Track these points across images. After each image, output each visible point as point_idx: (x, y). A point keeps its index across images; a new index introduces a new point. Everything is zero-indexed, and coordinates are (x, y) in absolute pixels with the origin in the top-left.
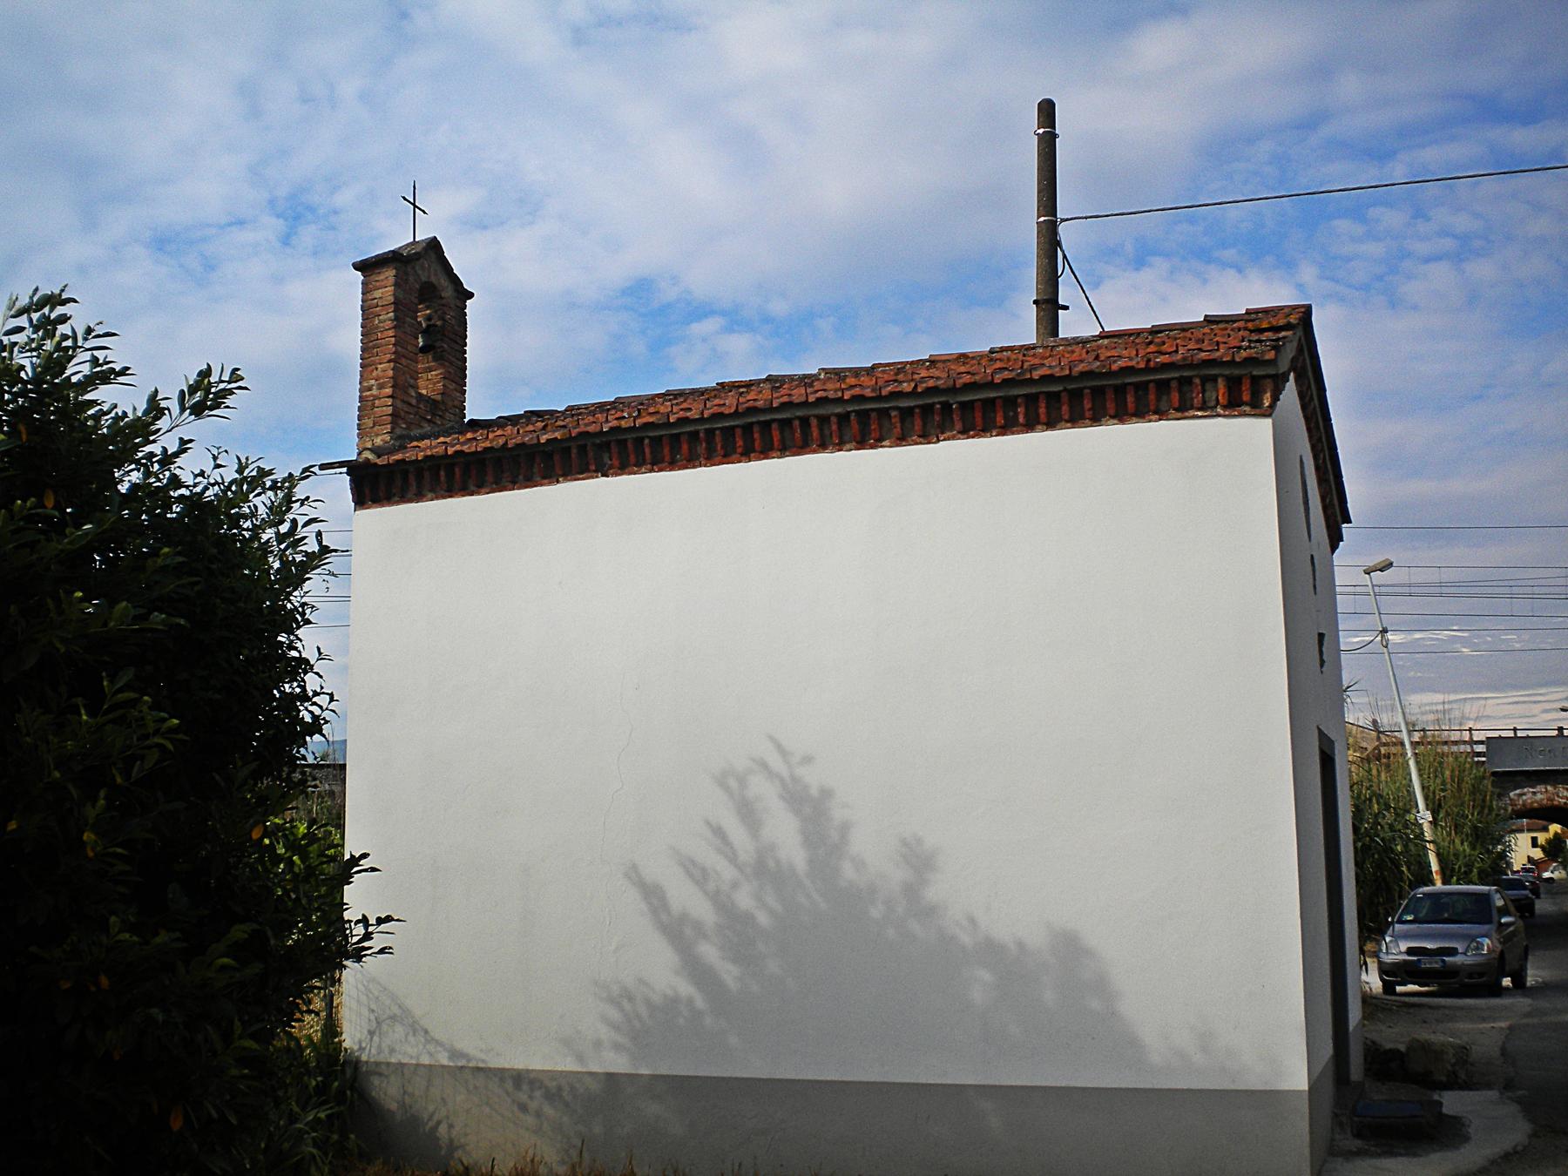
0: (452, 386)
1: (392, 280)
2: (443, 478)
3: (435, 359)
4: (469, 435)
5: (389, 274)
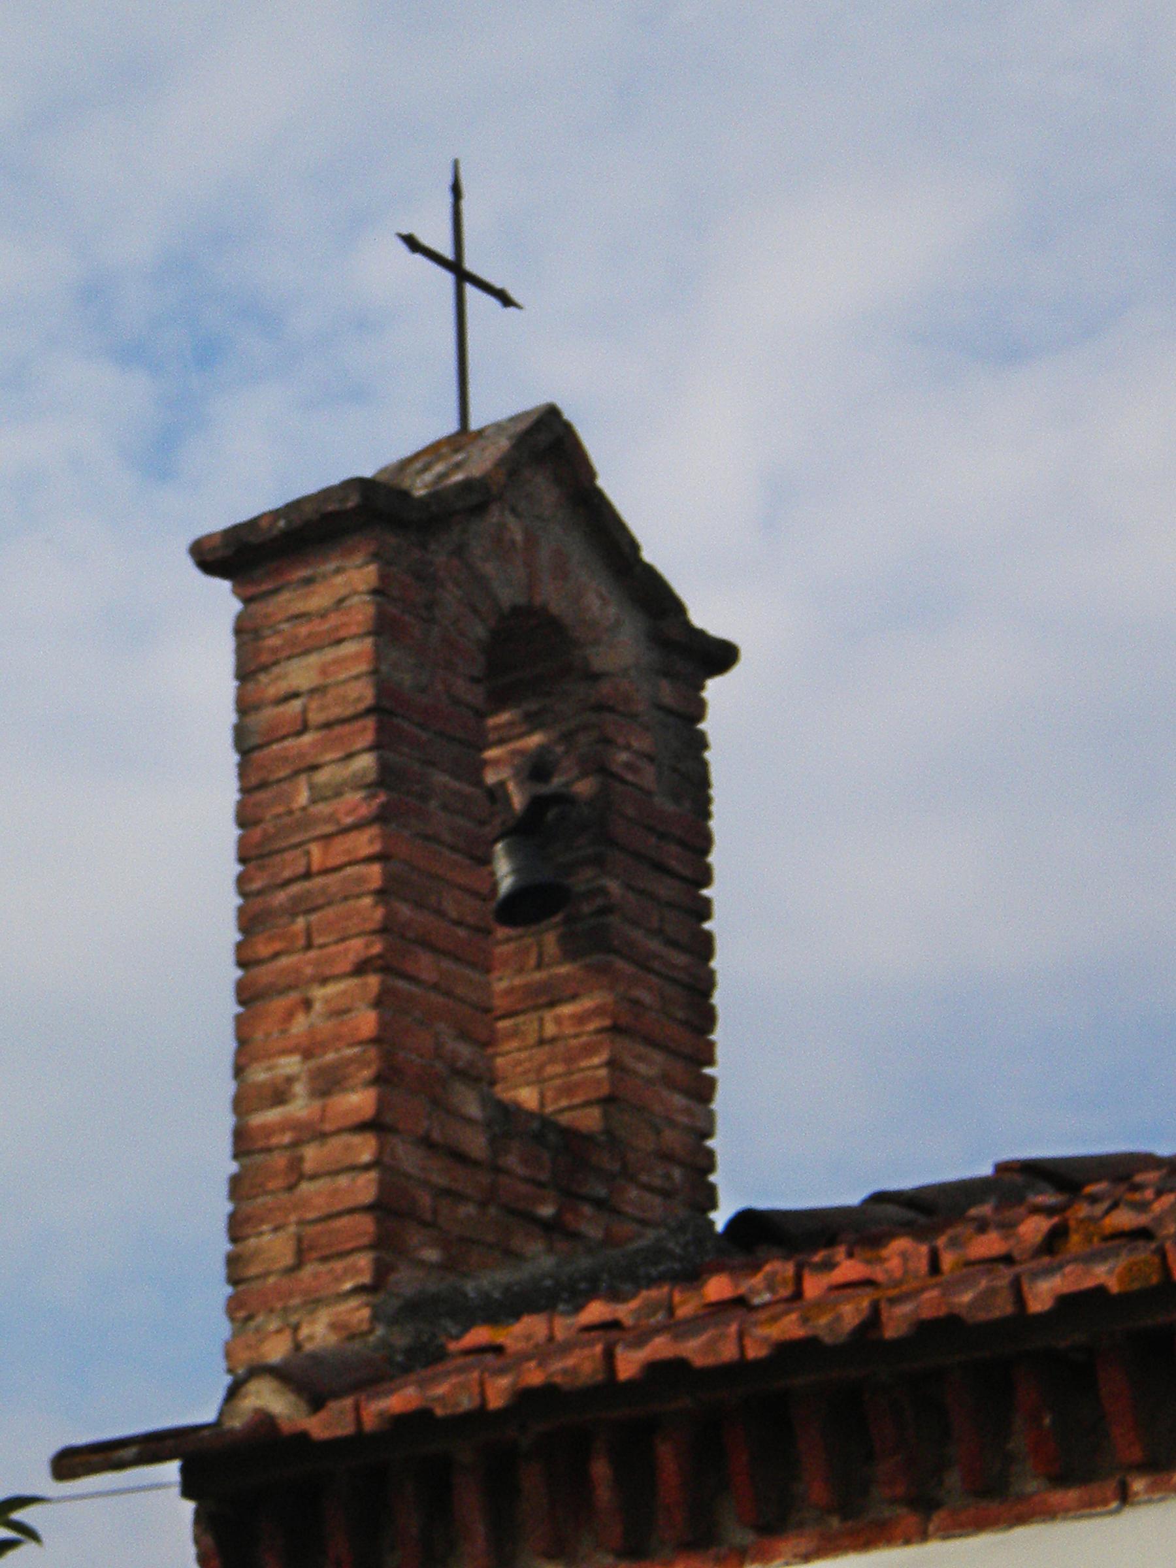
0: (649, 1065)
1: (362, 611)
2: (604, 1495)
3: (570, 952)
4: (717, 1287)
5: (347, 582)
